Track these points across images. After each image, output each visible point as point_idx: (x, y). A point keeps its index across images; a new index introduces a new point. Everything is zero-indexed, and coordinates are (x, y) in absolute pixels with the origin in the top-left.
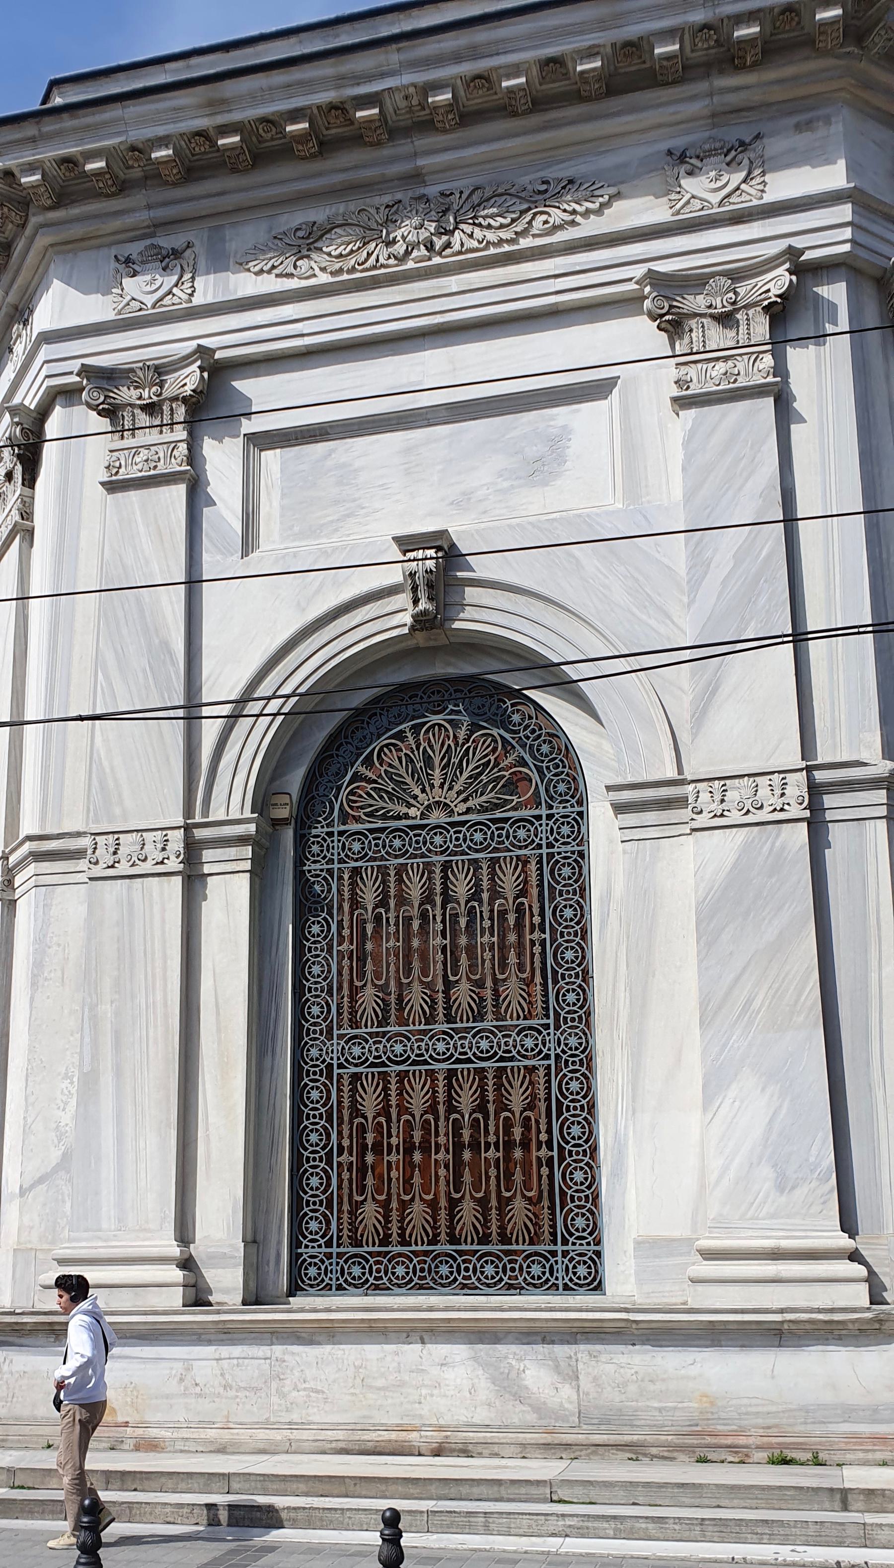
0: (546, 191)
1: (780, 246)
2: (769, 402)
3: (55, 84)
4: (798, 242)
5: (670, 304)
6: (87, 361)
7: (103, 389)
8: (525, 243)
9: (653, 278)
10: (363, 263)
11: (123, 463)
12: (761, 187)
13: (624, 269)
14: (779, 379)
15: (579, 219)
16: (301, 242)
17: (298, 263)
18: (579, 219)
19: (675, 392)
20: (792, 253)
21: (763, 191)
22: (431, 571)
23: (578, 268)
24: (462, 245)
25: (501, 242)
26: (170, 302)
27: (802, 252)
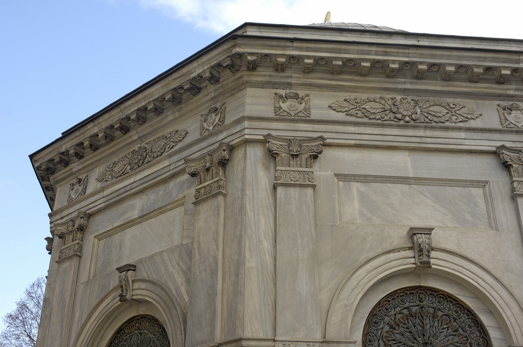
3: (246, 25)
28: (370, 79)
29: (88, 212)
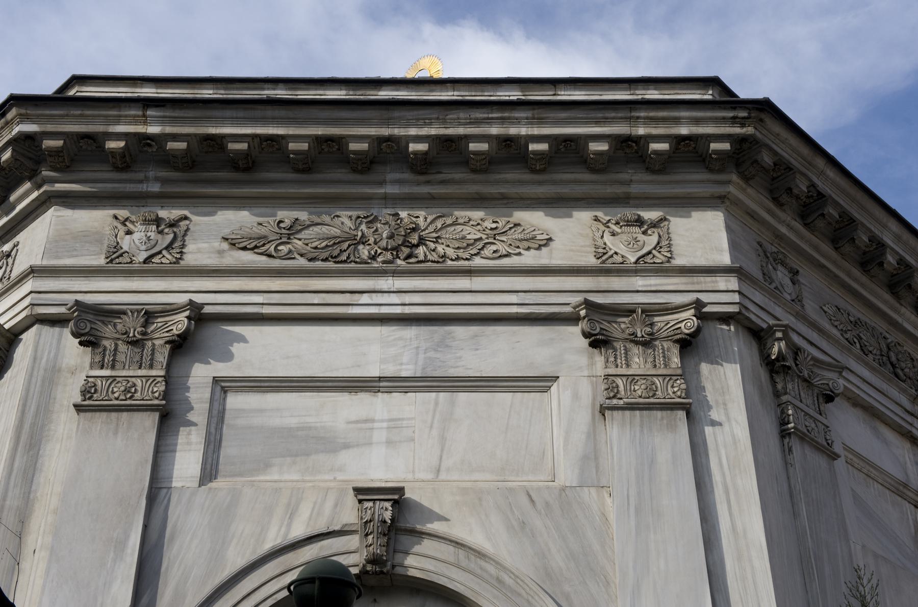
0: (496, 228)
1: (691, 297)
2: (156, 416)
3: (77, 80)
4: (704, 298)
5: (602, 327)
6: (80, 297)
7: (88, 324)
8: (478, 262)
9: (588, 304)
10: (336, 257)
11: (139, 389)
12: (178, 256)
13: (566, 292)
14: (164, 402)
15: (522, 251)
16: (284, 231)
17: (280, 248)
18: (522, 251)
19: (78, 399)
20: (698, 305)
21: (180, 259)
22: (385, 522)
23: (649, 289)
24: (426, 256)
25: (458, 258)
26: (159, 261)
27: (705, 305)
28: (498, 176)
29: (207, 310)
